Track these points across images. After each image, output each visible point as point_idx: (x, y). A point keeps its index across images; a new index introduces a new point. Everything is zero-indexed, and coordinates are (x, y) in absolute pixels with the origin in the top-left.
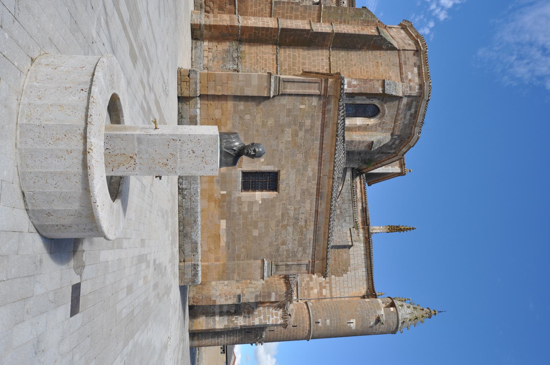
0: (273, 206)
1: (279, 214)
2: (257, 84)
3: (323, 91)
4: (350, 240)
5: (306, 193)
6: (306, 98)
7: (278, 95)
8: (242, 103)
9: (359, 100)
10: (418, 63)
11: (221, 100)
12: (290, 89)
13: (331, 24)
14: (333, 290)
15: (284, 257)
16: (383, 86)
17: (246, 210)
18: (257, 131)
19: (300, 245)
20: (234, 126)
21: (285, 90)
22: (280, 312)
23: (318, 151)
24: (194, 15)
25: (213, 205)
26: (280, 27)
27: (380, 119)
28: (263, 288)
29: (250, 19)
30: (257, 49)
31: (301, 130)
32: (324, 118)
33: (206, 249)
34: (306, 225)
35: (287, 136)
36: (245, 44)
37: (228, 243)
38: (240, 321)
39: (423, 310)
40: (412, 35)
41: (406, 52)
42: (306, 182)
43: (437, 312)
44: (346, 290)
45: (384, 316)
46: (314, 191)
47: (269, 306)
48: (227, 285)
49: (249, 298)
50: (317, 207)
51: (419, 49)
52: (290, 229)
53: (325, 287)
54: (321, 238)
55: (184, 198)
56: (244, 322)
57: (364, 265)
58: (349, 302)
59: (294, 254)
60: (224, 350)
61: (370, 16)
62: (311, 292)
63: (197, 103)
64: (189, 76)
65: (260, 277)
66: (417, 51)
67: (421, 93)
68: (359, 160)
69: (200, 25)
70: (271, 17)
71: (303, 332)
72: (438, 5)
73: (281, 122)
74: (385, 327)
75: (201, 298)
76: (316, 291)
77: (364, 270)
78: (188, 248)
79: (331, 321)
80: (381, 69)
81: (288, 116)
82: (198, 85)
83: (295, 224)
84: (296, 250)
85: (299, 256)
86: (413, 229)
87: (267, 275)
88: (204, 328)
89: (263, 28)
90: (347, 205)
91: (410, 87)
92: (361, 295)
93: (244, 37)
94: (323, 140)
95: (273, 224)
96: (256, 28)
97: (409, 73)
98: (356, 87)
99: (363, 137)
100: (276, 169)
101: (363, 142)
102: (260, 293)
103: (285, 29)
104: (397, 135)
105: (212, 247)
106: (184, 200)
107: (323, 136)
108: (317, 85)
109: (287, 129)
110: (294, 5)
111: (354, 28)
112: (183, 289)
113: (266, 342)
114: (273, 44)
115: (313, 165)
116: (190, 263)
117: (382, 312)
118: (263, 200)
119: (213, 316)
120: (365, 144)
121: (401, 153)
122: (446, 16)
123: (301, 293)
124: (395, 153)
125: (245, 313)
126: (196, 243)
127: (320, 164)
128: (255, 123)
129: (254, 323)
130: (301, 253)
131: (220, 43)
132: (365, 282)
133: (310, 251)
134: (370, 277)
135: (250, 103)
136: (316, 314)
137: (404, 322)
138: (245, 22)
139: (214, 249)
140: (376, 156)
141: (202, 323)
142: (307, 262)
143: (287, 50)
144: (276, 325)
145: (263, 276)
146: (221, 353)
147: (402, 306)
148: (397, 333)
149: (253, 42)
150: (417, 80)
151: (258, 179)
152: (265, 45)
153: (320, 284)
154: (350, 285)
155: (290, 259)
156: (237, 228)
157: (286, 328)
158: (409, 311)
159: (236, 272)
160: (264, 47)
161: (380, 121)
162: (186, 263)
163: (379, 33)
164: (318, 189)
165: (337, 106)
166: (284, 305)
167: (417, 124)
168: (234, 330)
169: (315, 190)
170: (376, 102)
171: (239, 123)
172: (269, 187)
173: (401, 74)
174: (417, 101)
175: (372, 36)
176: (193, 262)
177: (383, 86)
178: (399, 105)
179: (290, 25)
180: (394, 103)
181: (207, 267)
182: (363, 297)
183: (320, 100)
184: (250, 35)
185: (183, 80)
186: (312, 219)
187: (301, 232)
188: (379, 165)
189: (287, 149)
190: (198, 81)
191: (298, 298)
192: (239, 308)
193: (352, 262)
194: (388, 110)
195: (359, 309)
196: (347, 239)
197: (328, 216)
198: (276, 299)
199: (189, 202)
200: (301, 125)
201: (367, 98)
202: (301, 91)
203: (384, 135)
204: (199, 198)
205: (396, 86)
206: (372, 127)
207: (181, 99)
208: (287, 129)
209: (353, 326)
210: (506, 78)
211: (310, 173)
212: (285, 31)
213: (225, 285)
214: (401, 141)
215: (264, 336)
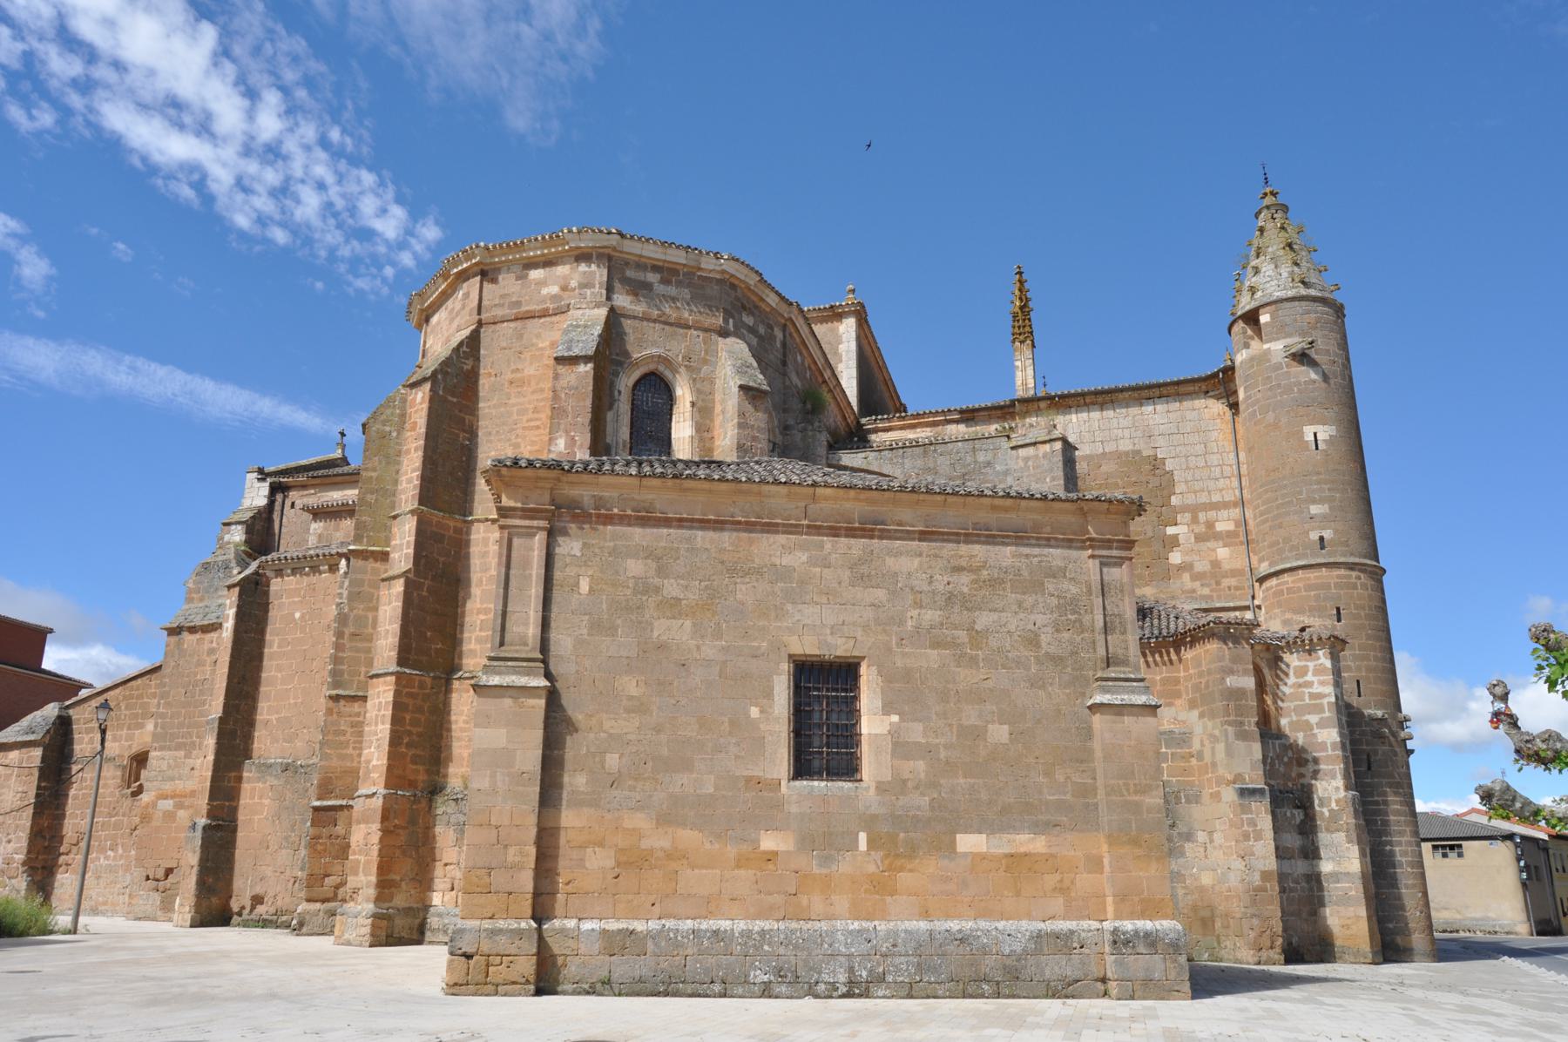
0: (908, 675)
3: (535, 523)
4: (1047, 447)
5: (864, 569)
6: (558, 575)
8: (566, 779)
9: (616, 431)
10: (517, 269)
11: (557, 847)
12: (526, 624)
13: (395, 517)
14: (1216, 498)
15: (1078, 639)
16: (573, 360)
17: (921, 765)
18: (658, 730)
19: (1037, 587)
20: (640, 807)
21: (530, 641)
22: (1293, 660)
23: (726, 535)
24: (346, 936)
25: (904, 879)
26: (393, 668)
27: (675, 371)
28: (1212, 716)
29: (368, 762)
30: (459, 739)
31: (657, 590)
32: (623, 520)
34: (971, 570)
35: (677, 631)
36: (445, 776)
37: (1039, 828)
38: (1332, 791)
39: (1262, 230)
40: (443, 293)
41: (485, 303)
43: (1268, 190)
44: (1214, 459)
45: (1289, 341)
46: (857, 545)
47: (1275, 697)
48: (1211, 833)
49: (1248, 761)
50: (908, 536)
51: (476, 269)
52: (984, 620)
53: (1210, 525)
54: (1013, 518)
55: (881, 979)
56: (1334, 777)
57: (1134, 411)
58: (1250, 450)
59: (1070, 604)
60: (1452, 848)
61: (389, 412)
62: (1226, 566)
63: (563, 931)
64: (469, 957)
65: (1150, 720)
67: (600, 257)
68: (804, 430)
69: (375, 916)
70: (364, 699)
71: (1355, 587)
72: (402, 245)
74: (1324, 336)
75: (1255, 922)
76: (1223, 553)
77: (1150, 408)
78: (1056, 967)
79: (1314, 502)
80: (530, 371)
81: (612, 631)
82: (501, 924)
83: (968, 604)
84: (1055, 601)
86: (1020, 273)
87: (1140, 693)
88: (1363, 912)
89: (396, 720)
90: (940, 460)
91: (583, 286)
92: (1229, 413)
93: (422, 777)
94: (692, 520)
95: (966, 677)
96: (395, 740)
97: (545, 291)
98: (573, 438)
99: (728, 415)
100: (785, 667)
101: (742, 414)
102: (1230, 723)
103: (399, 653)
104: (726, 321)
105: (1051, 880)
106: (890, 978)
107: (681, 520)
108: (516, 541)
110: (347, 631)
111: (408, 452)
112: (1208, 982)
113: (1398, 708)
114: (448, 691)
116: (1110, 959)
118: (887, 709)
119: (1319, 882)
120: (750, 408)
121: (783, 308)
122: (430, 221)
123: (1234, 598)
124: (784, 328)
125: (1302, 776)
126: (1039, 936)
127: (770, 528)
128: (630, 737)
129: (1334, 744)
130: (1065, 585)
131: (438, 856)
132: (1187, 404)
133: (1056, 555)
134: (1171, 390)
135: (569, 755)
136: (1293, 548)
137: (1303, 282)
138: (375, 775)
139: (1058, 876)
140: (795, 380)
141: (1346, 916)
142: (1093, 565)
143: (466, 647)
144: (1337, 672)
145: (1144, 706)
146: (1460, 855)
147: (1253, 290)
148: (1340, 300)
149: (439, 750)
150: (562, 270)
151: (820, 726)
152: (449, 713)
153: (1199, 538)
154: (1200, 449)
155: (1086, 619)
156: (984, 796)
157: (1344, 642)
158: (1267, 269)
160: (453, 718)
161: (682, 370)
162: (1109, 975)
163: (425, 380)
164: (851, 533)
165: (585, 477)
166: (1268, 647)
167: (692, 263)
168: (1365, 813)
169: (853, 541)
170: (626, 382)
172: (846, 691)
173: (544, 314)
174: (621, 270)
175: (434, 400)
176: (1107, 949)
177: (573, 360)
178: (635, 318)
179: (390, 639)
180: (628, 330)
181: (1121, 898)
182: (1234, 406)
183: (565, 533)
184: (415, 760)
185: (481, 978)
186: (948, 549)
188: (827, 374)
189: (718, 635)
190: (487, 924)
191: (1247, 608)
192: (1288, 793)
193: (1125, 446)
194: (646, 345)
195: (1271, 417)
197: (939, 498)
198: (1245, 672)
199: (897, 960)
200: (645, 588)
201: (611, 408)
202: (535, 591)
203: (723, 355)
204: (882, 926)
205: (578, 326)
206: (699, 392)
207: (545, 983)
208: (656, 634)
209: (1325, 432)
210: (581, 48)
212: (405, 655)
213: (1212, 841)
214: (744, 307)
215: (1379, 713)
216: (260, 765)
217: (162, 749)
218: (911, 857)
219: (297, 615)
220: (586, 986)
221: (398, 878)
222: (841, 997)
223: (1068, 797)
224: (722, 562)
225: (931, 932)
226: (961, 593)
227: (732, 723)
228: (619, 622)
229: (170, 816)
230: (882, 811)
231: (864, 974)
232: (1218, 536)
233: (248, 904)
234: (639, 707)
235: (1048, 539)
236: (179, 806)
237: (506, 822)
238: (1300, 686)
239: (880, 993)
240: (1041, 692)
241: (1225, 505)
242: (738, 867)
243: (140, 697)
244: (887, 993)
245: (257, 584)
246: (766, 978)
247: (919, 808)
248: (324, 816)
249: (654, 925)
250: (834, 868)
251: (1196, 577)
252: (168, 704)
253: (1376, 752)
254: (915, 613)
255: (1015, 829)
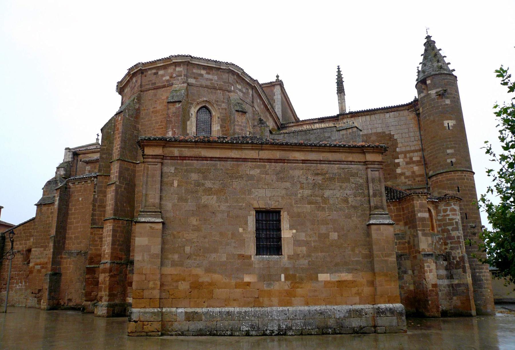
0: (299, 215)
1: (308, 208)
2: (147, 239)
3: (157, 160)
5: (282, 175)
7: (161, 212)
13: (111, 162)
15: (363, 199)
17: (304, 249)
20: (199, 266)
25: (299, 291)
29: (105, 251)
31: (203, 185)
33: (357, 299)
34: (322, 174)
35: (211, 200)
37: (349, 271)
41: (143, 84)
42: (267, 176)
52: (327, 193)
53: (411, 158)
62: (417, 173)
66: (142, 73)
73: (195, 209)
76: (416, 168)
79: (448, 148)
81: (186, 200)
82: (147, 310)
83: (321, 187)
84: (354, 185)
85: (361, 181)
89: (114, 236)
95: (321, 215)
96: (113, 243)
97: (164, 79)
103: (114, 211)
105: (354, 290)
109: (203, 201)
115: (246, 169)
117: (433, 92)
118: (291, 228)
128: (195, 240)
153: (407, 163)
154: (406, 131)
159: (386, 258)
169: (277, 164)
171: (195, 259)
173: (164, 86)
179: (111, 207)
184: (121, 250)
185: (140, 330)
187: (331, 179)
190: (142, 310)
191: (425, 188)
193: (379, 130)
196: (350, 133)
198: (425, 212)
199: (296, 321)
200: (198, 184)
201: (189, 120)
204: (291, 309)
208: (203, 201)
211: (256, 172)
216: (69, 253)
217: (36, 247)
218: (301, 283)
219: (80, 199)
220: (180, 333)
221: (116, 293)
222: (275, 335)
223: (360, 259)
224: (228, 174)
225: (309, 311)
226: (319, 183)
227: (232, 234)
228: (189, 197)
229: (39, 271)
230: (290, 266)
231: (284, 327)
232: (414, 162)
233: (66, 302)
234: (197, 229)
235: (351, 162)
236: (42, 268)
237: (148, 272)
238: (445, 216)
239: (290, 334)
240: (349, 220)
241: (416, 151)
242: (236, 288)
243: (28, 229)
244: (293, 333)
245: (66, 188)
246: (247, 329)
247: (304, 265)
248: (91, 271)
249: (204, 310)
250: (272, 287)
251: (406, 178)
252: (37, 232)
253: (473, 239)
254: (301, 191)
255: (341, 272)
